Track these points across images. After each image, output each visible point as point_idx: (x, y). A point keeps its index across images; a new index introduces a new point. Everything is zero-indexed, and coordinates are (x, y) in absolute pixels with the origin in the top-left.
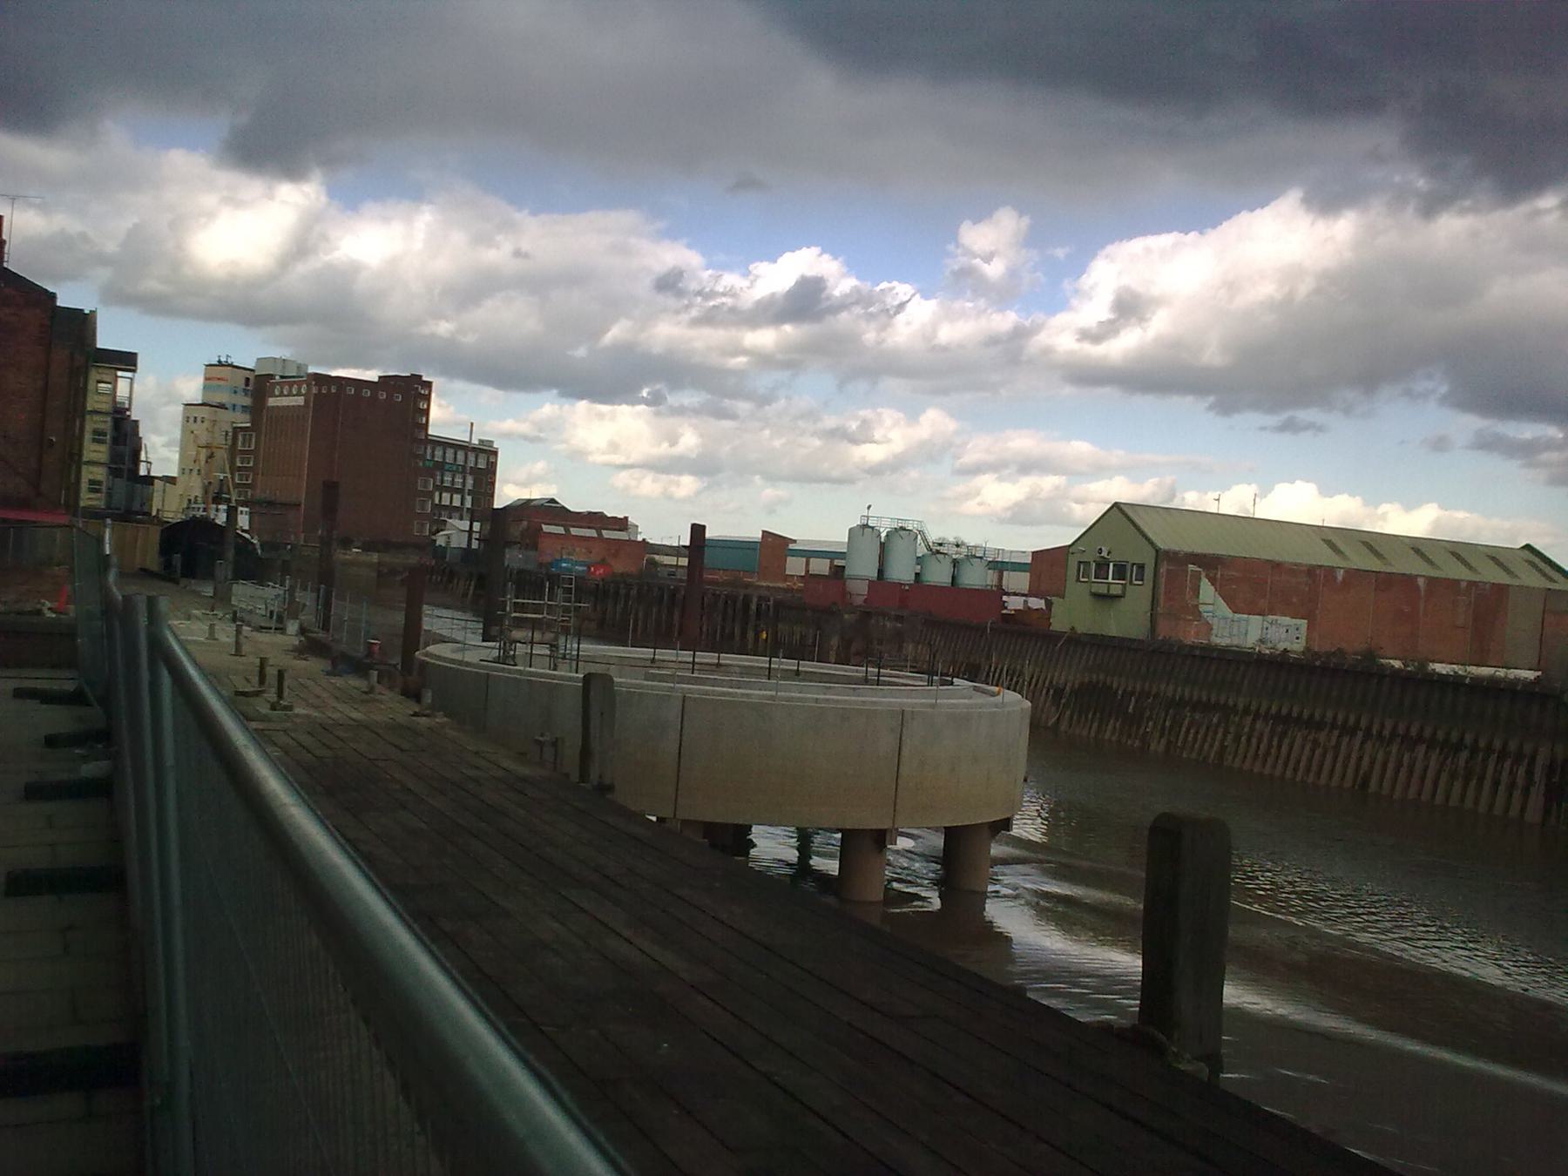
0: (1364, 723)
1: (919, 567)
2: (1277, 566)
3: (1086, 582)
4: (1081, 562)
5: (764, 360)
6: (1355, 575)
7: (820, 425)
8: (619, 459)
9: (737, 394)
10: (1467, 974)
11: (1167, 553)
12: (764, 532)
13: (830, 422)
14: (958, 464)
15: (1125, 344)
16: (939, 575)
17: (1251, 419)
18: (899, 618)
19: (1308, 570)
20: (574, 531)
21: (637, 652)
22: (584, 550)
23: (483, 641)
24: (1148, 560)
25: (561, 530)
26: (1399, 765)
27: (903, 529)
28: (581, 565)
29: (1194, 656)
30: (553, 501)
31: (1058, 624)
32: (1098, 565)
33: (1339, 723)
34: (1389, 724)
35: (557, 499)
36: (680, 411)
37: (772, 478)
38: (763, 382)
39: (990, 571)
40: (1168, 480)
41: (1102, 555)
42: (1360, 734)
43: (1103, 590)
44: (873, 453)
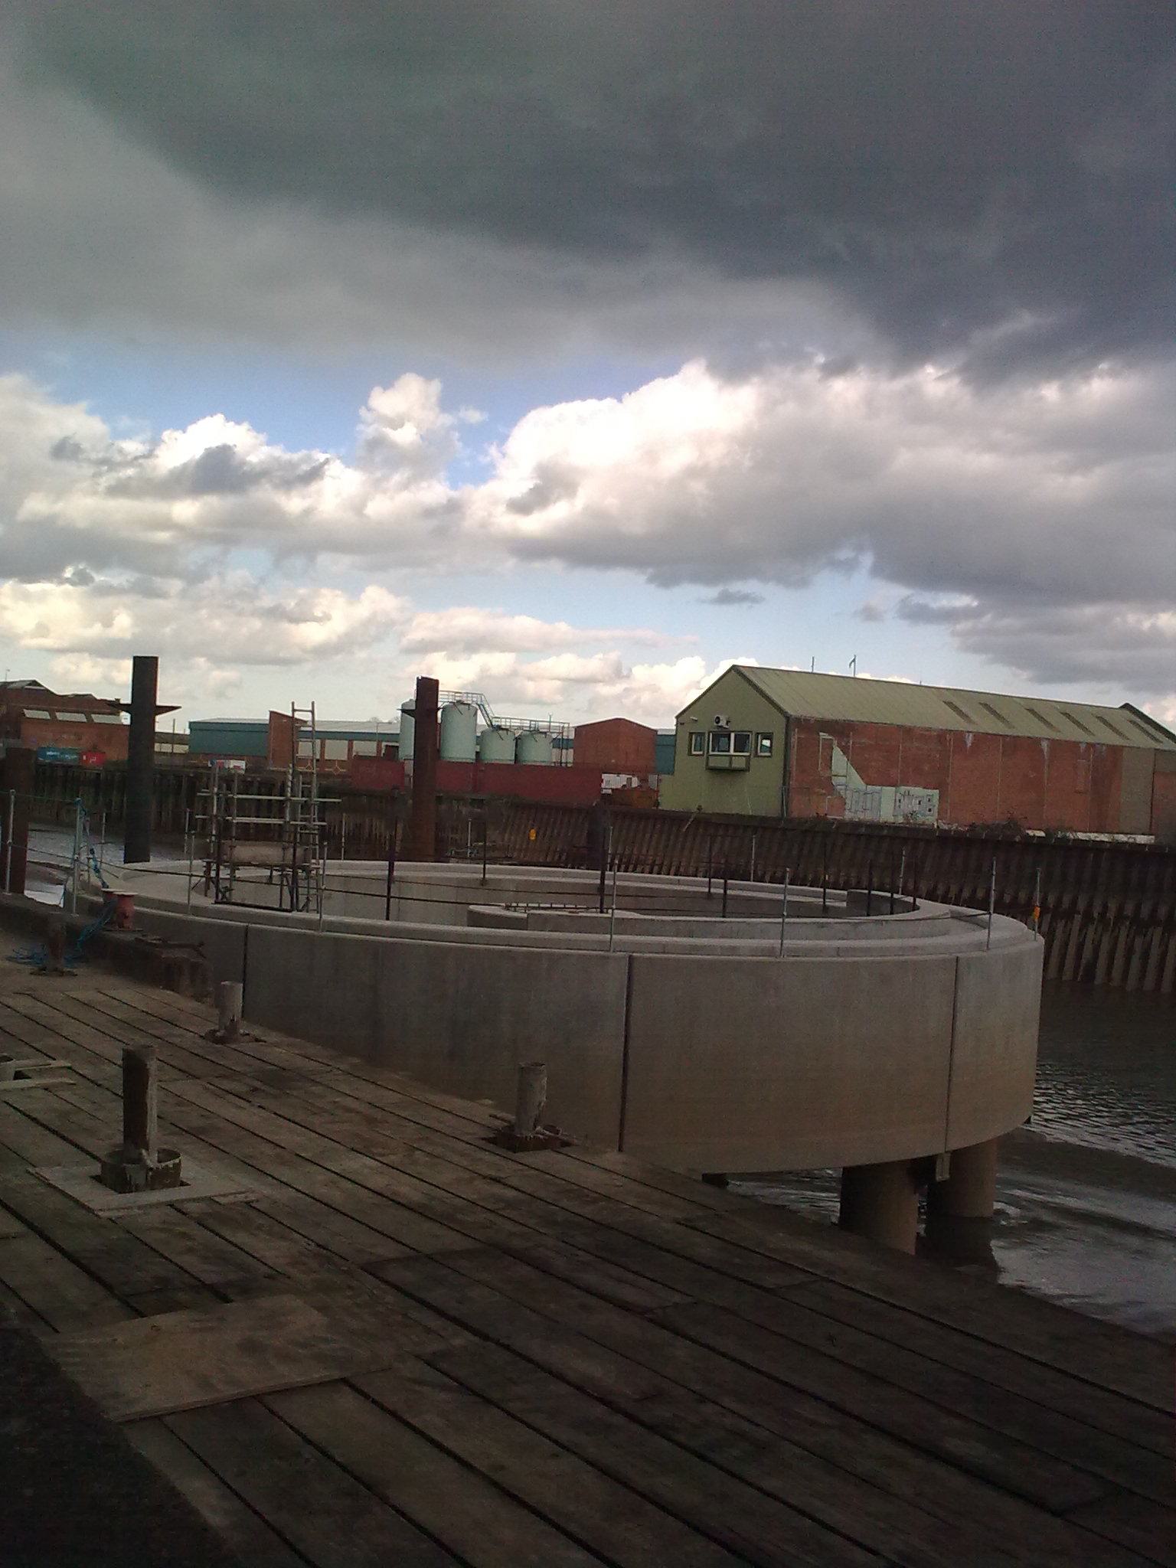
0: (1081, 905)
1: (478, 747)
2: (908, 731)
3: (769, 757)
4: (692, 733)
5: (191, 534)
6: (982, 738)
7: (258, 604)
8: (48, 642)
9: (169, 572)
10: (1104, 1148)
11: (798, 720)
12: (272, 713)
13: (267, 601)
14: (405, 641)
15: (556, 515)
16: (501, 753)
17: (690, 592)
18: (480, 803)
19: (938, 735)
20: (60, 716)
21: (357, 868)
22: (72, 737)
23: (125, 862)
24: (778, 727)
25: (45, 715)
26: (1129, 952)
27: (460, 702)
28: (69, 753)
29: (859, 836)
30: (35, 683)
31: (669, 802)
32: (717, 737)
33: (1051, 906)
34: (1113, 906)
35: (39, 681)
36: (105, 591)
37: (219, 660)
38: (195, 556)
39: (554, 750)
40: (613, 656)
41: (720, 724)
42: (1078, 918)
43: (723, 763)
44: (312, 633)
